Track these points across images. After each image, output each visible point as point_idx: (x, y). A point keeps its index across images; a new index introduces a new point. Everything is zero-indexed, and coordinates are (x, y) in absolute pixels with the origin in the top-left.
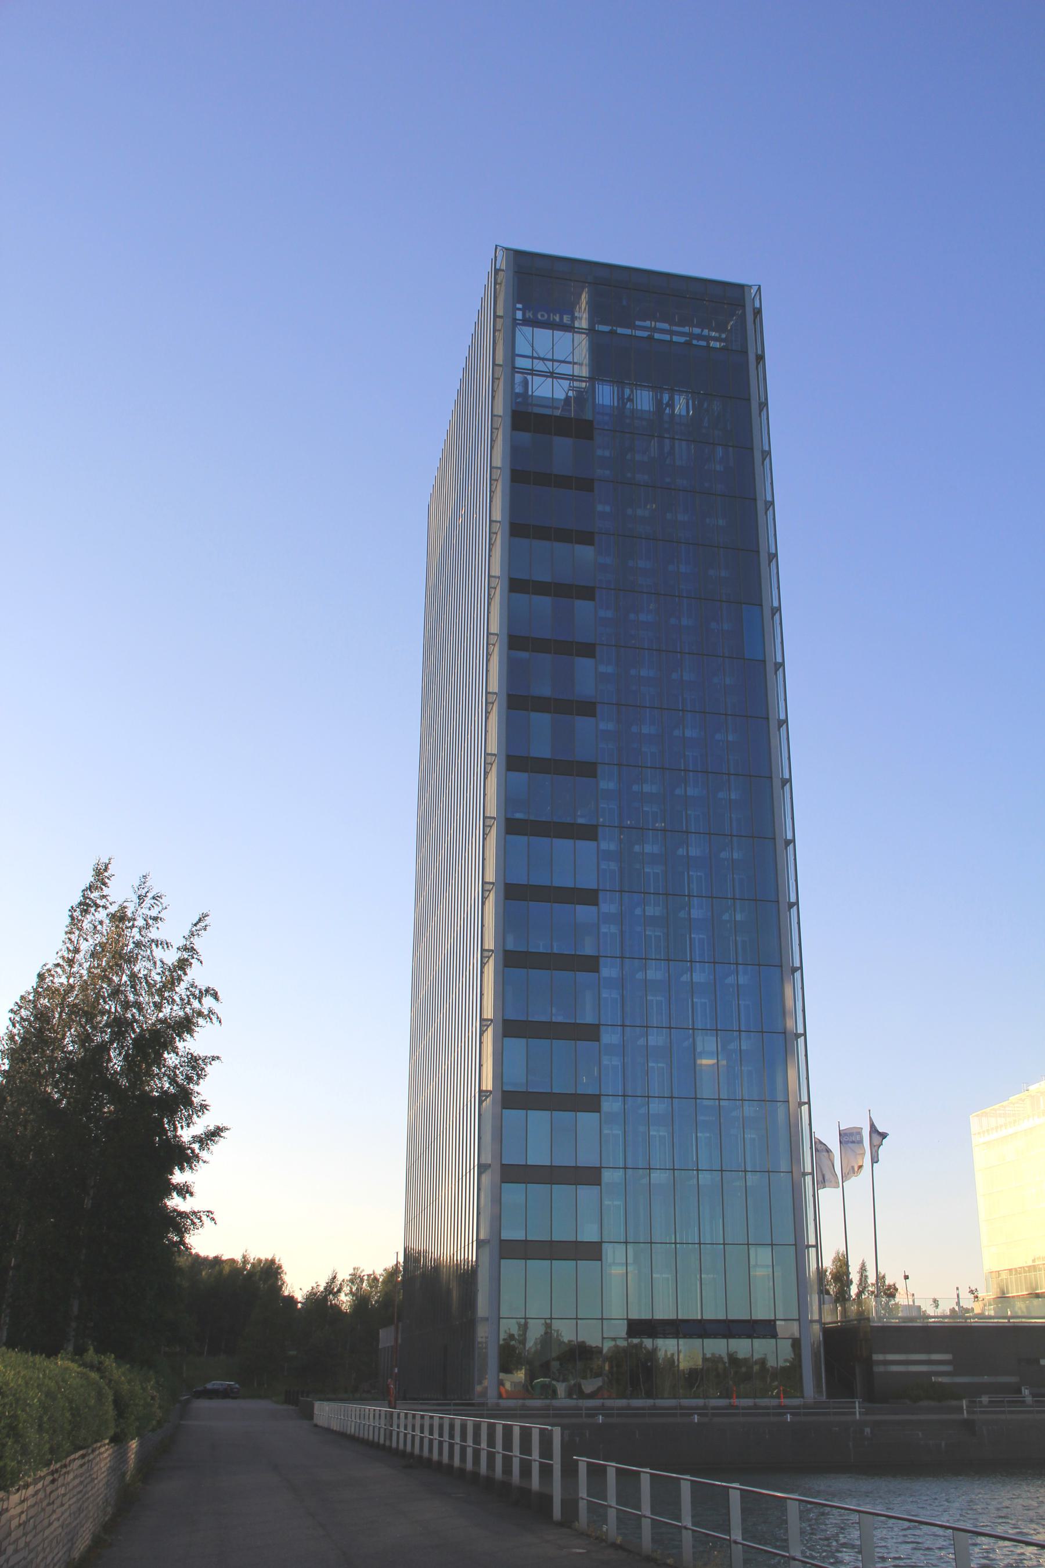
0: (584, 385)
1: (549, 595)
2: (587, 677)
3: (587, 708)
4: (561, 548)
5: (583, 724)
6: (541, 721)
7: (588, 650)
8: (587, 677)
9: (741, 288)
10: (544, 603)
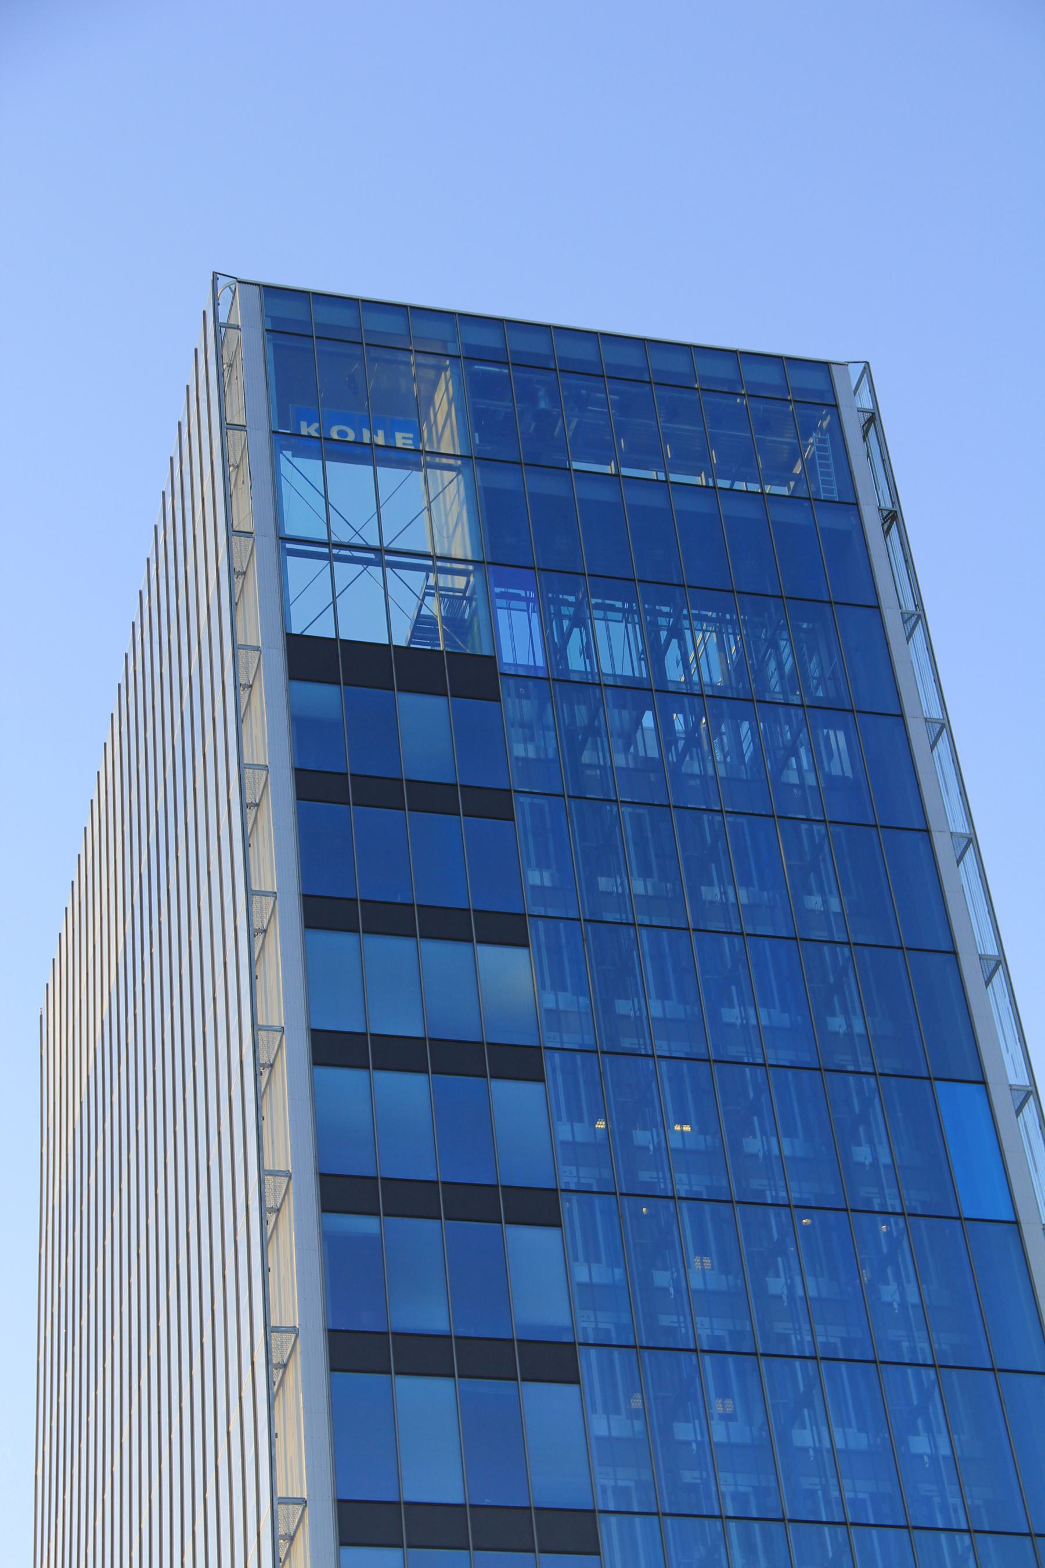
0: (460, 582)
1: (420, 1069)
2: (543, 1279)
3: (553, 1360)
4: (439, 953)
5: (545, 1403)
6: (427, 1403)
7: (538, 1207)
8: (543, 1279)
9: (825, 366)
10: (409, 1091)
